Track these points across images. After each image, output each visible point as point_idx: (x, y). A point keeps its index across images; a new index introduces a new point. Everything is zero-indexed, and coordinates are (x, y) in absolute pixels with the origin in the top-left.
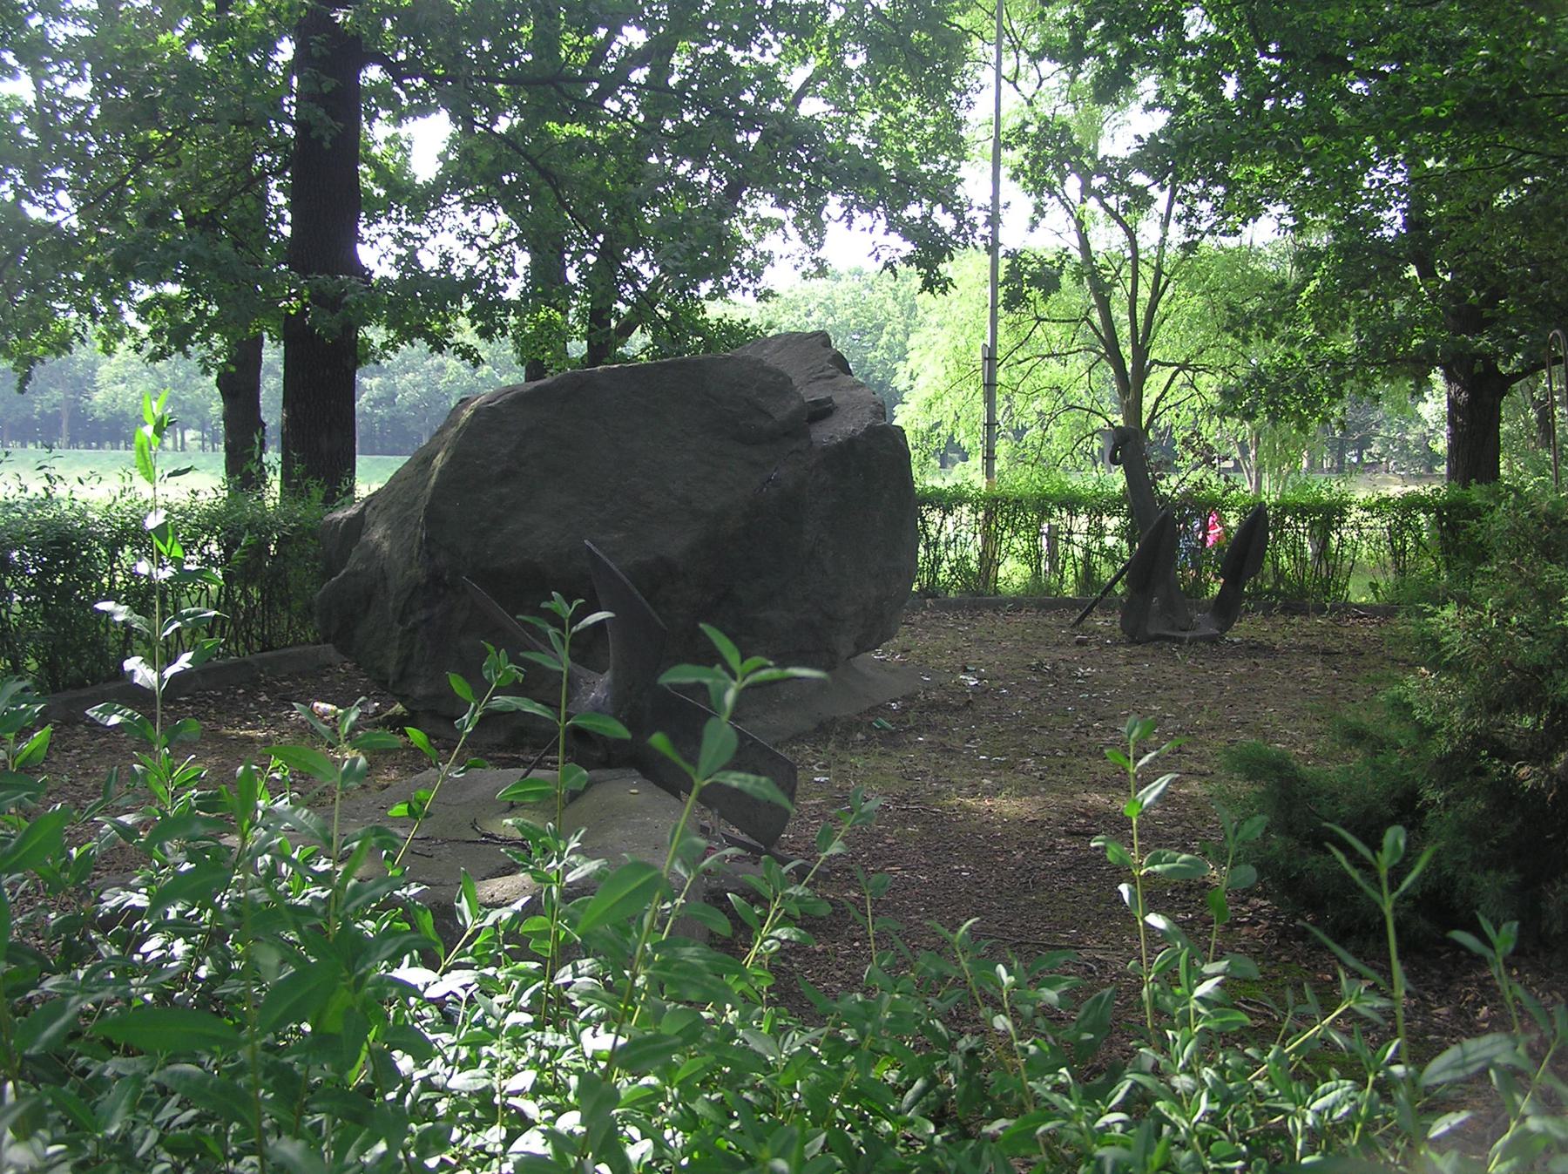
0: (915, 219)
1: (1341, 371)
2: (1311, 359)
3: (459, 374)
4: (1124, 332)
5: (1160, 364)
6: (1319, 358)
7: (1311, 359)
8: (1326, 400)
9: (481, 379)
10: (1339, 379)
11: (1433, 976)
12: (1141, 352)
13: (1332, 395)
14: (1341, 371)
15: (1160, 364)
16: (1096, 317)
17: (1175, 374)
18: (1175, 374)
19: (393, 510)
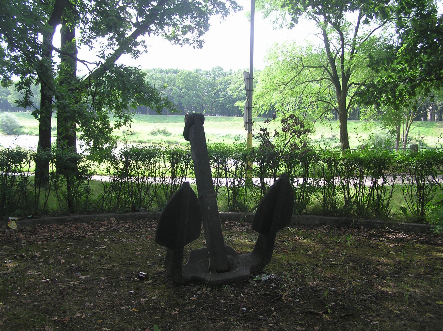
0: (292, 18)
1: (414, 83)
2: (400, 78)
3: (176, 91)
4: (339, 74)
5: (355, 84)
6: (404, 77)
7: (400, 78)
8: (407, 97)
9: (183, 93)
10: (413, 87)
11: (19, 25)
12: (346, 79)
13: (410, 94)
14: (414, 83)
15: (355, 84)
16: (330, 68)
17: (186, 173)
18: (186, 173)
19: (57, 59)
